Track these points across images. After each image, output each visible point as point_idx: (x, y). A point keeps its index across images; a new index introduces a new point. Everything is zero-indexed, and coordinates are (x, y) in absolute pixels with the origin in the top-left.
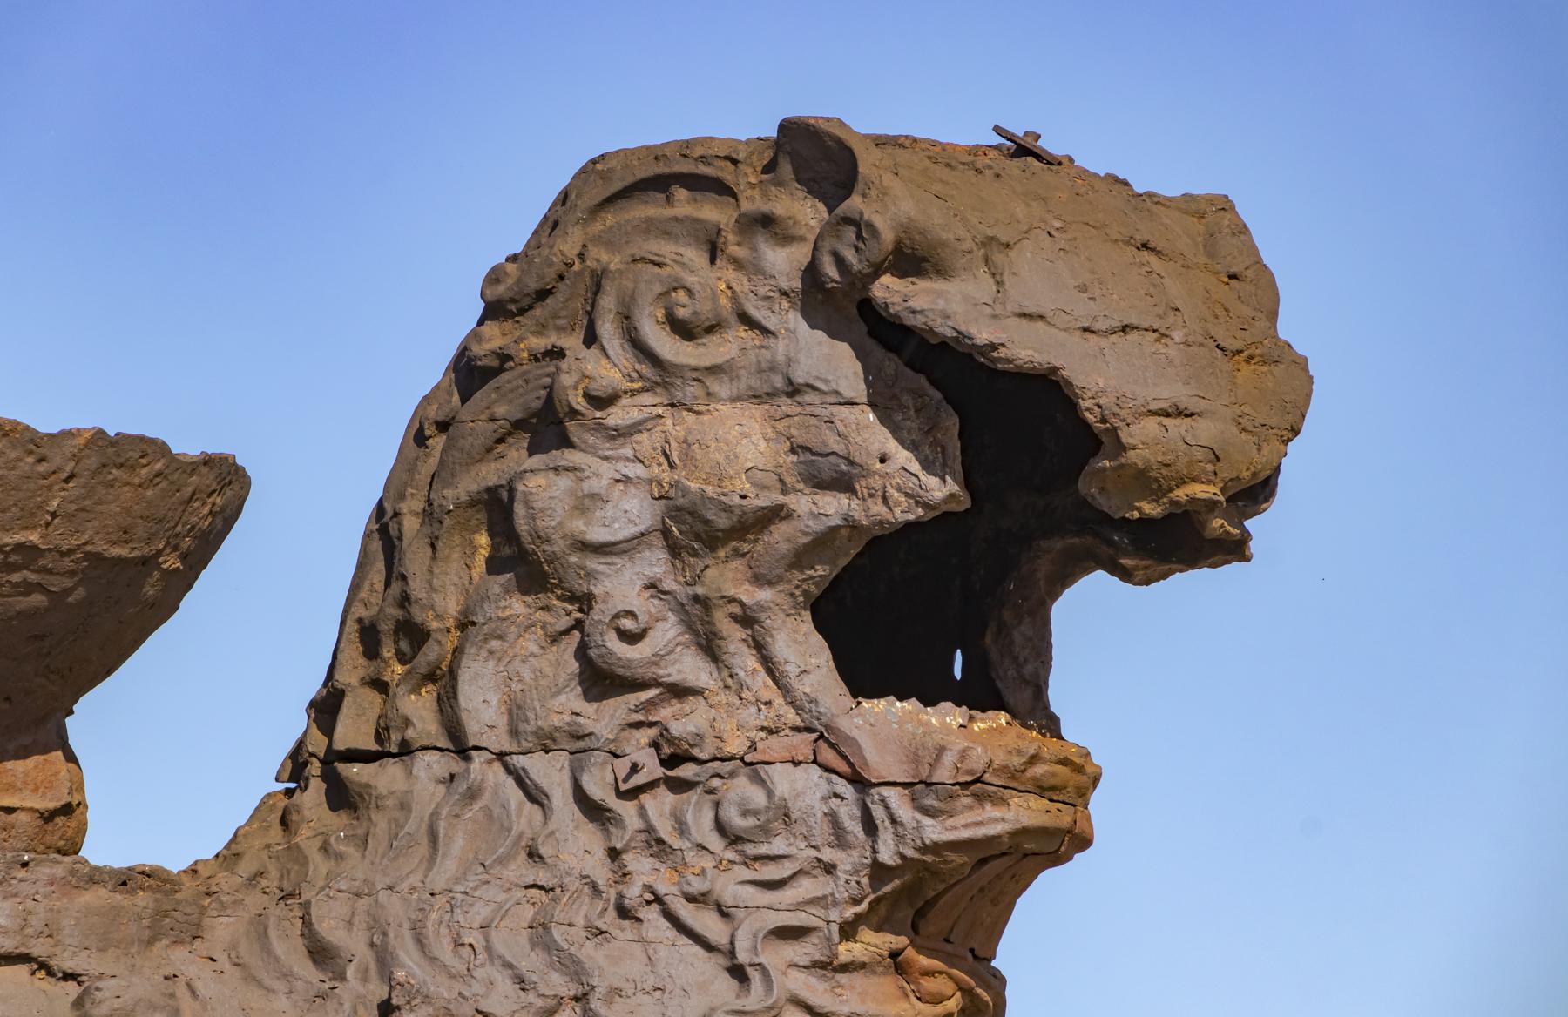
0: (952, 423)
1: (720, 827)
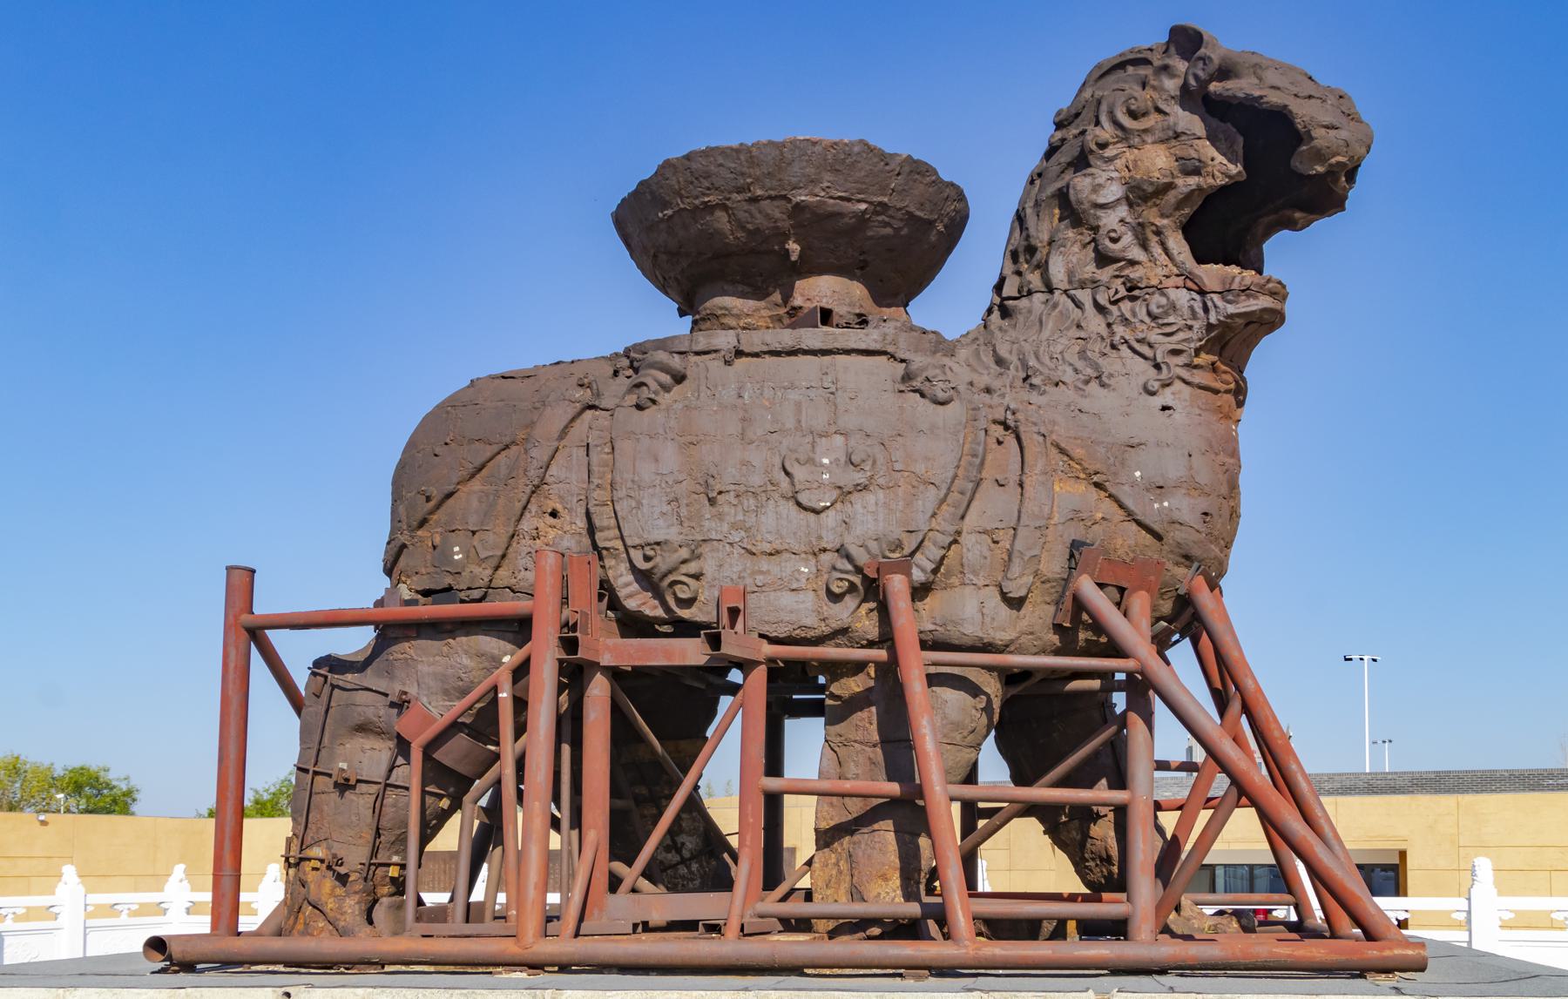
0: (1241, 140)
1: (1149, 314)
